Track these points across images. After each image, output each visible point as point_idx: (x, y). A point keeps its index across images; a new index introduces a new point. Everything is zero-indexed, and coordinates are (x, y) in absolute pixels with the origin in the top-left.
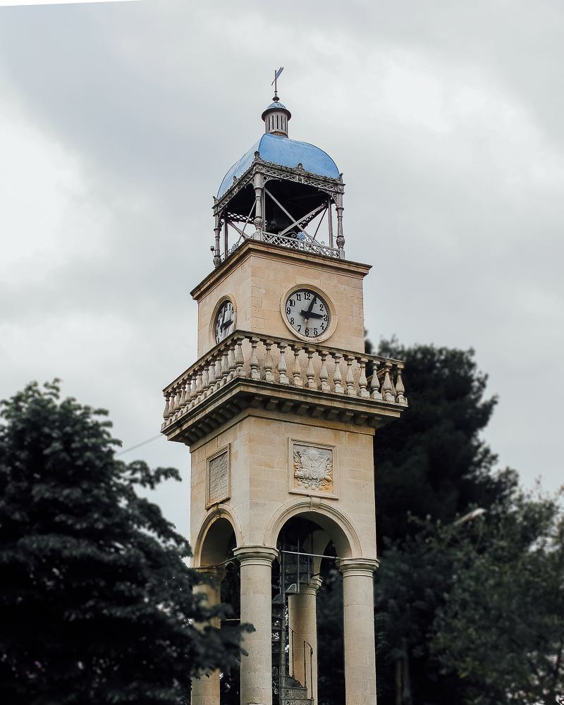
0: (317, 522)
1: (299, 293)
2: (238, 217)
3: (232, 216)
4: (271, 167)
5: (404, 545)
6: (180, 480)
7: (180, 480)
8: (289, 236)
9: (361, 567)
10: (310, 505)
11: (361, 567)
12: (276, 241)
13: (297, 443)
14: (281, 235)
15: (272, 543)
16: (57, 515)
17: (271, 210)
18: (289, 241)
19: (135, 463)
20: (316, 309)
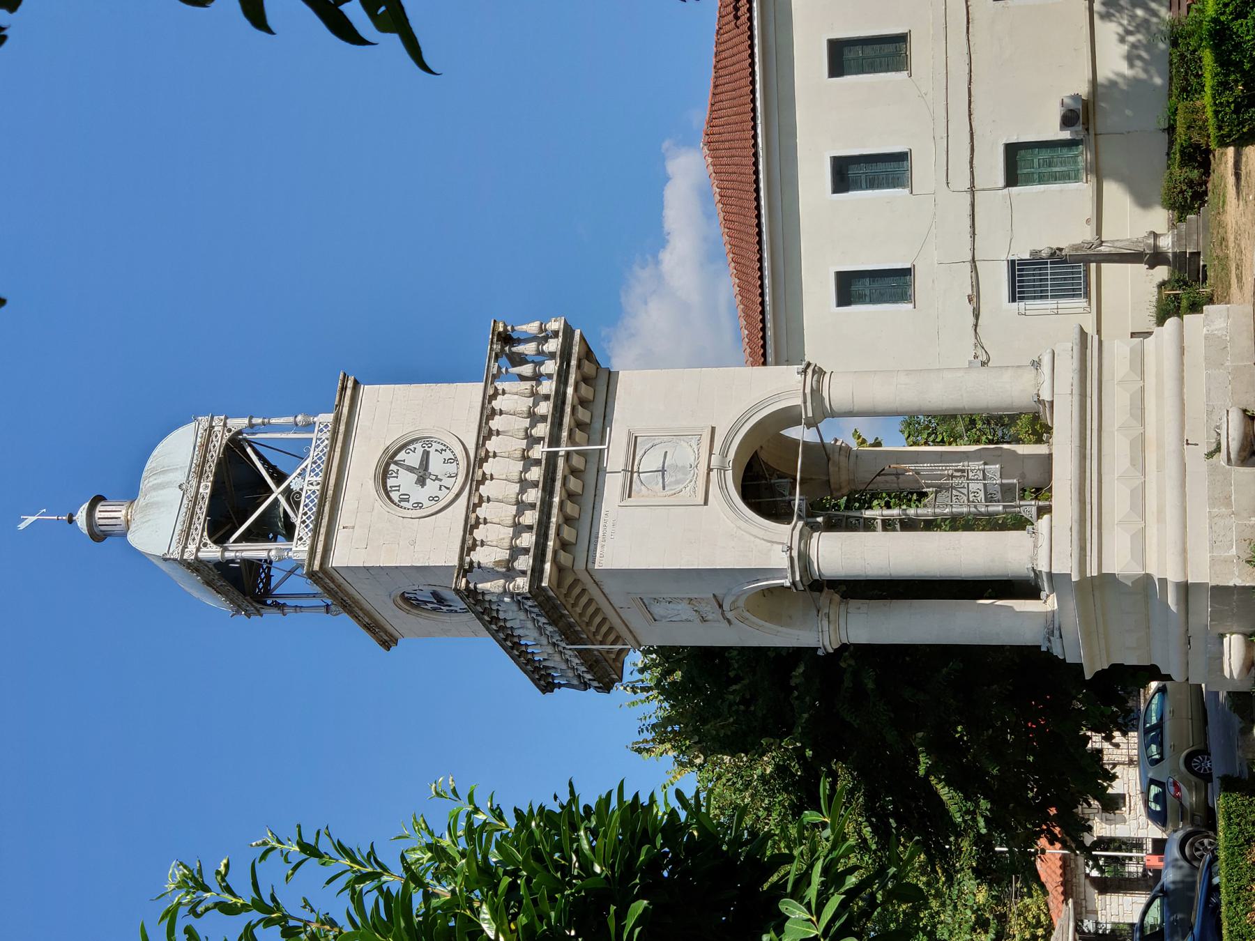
0: (746, 460)
1: (389, 489)
2: (263, 575)
3: (261, 585)
8: (298, 504)
12: (307, 526)
16: (1150, 876)
17: (259, 533)
18: (306, 506)
19: (520, 810)
20: (412, 458)
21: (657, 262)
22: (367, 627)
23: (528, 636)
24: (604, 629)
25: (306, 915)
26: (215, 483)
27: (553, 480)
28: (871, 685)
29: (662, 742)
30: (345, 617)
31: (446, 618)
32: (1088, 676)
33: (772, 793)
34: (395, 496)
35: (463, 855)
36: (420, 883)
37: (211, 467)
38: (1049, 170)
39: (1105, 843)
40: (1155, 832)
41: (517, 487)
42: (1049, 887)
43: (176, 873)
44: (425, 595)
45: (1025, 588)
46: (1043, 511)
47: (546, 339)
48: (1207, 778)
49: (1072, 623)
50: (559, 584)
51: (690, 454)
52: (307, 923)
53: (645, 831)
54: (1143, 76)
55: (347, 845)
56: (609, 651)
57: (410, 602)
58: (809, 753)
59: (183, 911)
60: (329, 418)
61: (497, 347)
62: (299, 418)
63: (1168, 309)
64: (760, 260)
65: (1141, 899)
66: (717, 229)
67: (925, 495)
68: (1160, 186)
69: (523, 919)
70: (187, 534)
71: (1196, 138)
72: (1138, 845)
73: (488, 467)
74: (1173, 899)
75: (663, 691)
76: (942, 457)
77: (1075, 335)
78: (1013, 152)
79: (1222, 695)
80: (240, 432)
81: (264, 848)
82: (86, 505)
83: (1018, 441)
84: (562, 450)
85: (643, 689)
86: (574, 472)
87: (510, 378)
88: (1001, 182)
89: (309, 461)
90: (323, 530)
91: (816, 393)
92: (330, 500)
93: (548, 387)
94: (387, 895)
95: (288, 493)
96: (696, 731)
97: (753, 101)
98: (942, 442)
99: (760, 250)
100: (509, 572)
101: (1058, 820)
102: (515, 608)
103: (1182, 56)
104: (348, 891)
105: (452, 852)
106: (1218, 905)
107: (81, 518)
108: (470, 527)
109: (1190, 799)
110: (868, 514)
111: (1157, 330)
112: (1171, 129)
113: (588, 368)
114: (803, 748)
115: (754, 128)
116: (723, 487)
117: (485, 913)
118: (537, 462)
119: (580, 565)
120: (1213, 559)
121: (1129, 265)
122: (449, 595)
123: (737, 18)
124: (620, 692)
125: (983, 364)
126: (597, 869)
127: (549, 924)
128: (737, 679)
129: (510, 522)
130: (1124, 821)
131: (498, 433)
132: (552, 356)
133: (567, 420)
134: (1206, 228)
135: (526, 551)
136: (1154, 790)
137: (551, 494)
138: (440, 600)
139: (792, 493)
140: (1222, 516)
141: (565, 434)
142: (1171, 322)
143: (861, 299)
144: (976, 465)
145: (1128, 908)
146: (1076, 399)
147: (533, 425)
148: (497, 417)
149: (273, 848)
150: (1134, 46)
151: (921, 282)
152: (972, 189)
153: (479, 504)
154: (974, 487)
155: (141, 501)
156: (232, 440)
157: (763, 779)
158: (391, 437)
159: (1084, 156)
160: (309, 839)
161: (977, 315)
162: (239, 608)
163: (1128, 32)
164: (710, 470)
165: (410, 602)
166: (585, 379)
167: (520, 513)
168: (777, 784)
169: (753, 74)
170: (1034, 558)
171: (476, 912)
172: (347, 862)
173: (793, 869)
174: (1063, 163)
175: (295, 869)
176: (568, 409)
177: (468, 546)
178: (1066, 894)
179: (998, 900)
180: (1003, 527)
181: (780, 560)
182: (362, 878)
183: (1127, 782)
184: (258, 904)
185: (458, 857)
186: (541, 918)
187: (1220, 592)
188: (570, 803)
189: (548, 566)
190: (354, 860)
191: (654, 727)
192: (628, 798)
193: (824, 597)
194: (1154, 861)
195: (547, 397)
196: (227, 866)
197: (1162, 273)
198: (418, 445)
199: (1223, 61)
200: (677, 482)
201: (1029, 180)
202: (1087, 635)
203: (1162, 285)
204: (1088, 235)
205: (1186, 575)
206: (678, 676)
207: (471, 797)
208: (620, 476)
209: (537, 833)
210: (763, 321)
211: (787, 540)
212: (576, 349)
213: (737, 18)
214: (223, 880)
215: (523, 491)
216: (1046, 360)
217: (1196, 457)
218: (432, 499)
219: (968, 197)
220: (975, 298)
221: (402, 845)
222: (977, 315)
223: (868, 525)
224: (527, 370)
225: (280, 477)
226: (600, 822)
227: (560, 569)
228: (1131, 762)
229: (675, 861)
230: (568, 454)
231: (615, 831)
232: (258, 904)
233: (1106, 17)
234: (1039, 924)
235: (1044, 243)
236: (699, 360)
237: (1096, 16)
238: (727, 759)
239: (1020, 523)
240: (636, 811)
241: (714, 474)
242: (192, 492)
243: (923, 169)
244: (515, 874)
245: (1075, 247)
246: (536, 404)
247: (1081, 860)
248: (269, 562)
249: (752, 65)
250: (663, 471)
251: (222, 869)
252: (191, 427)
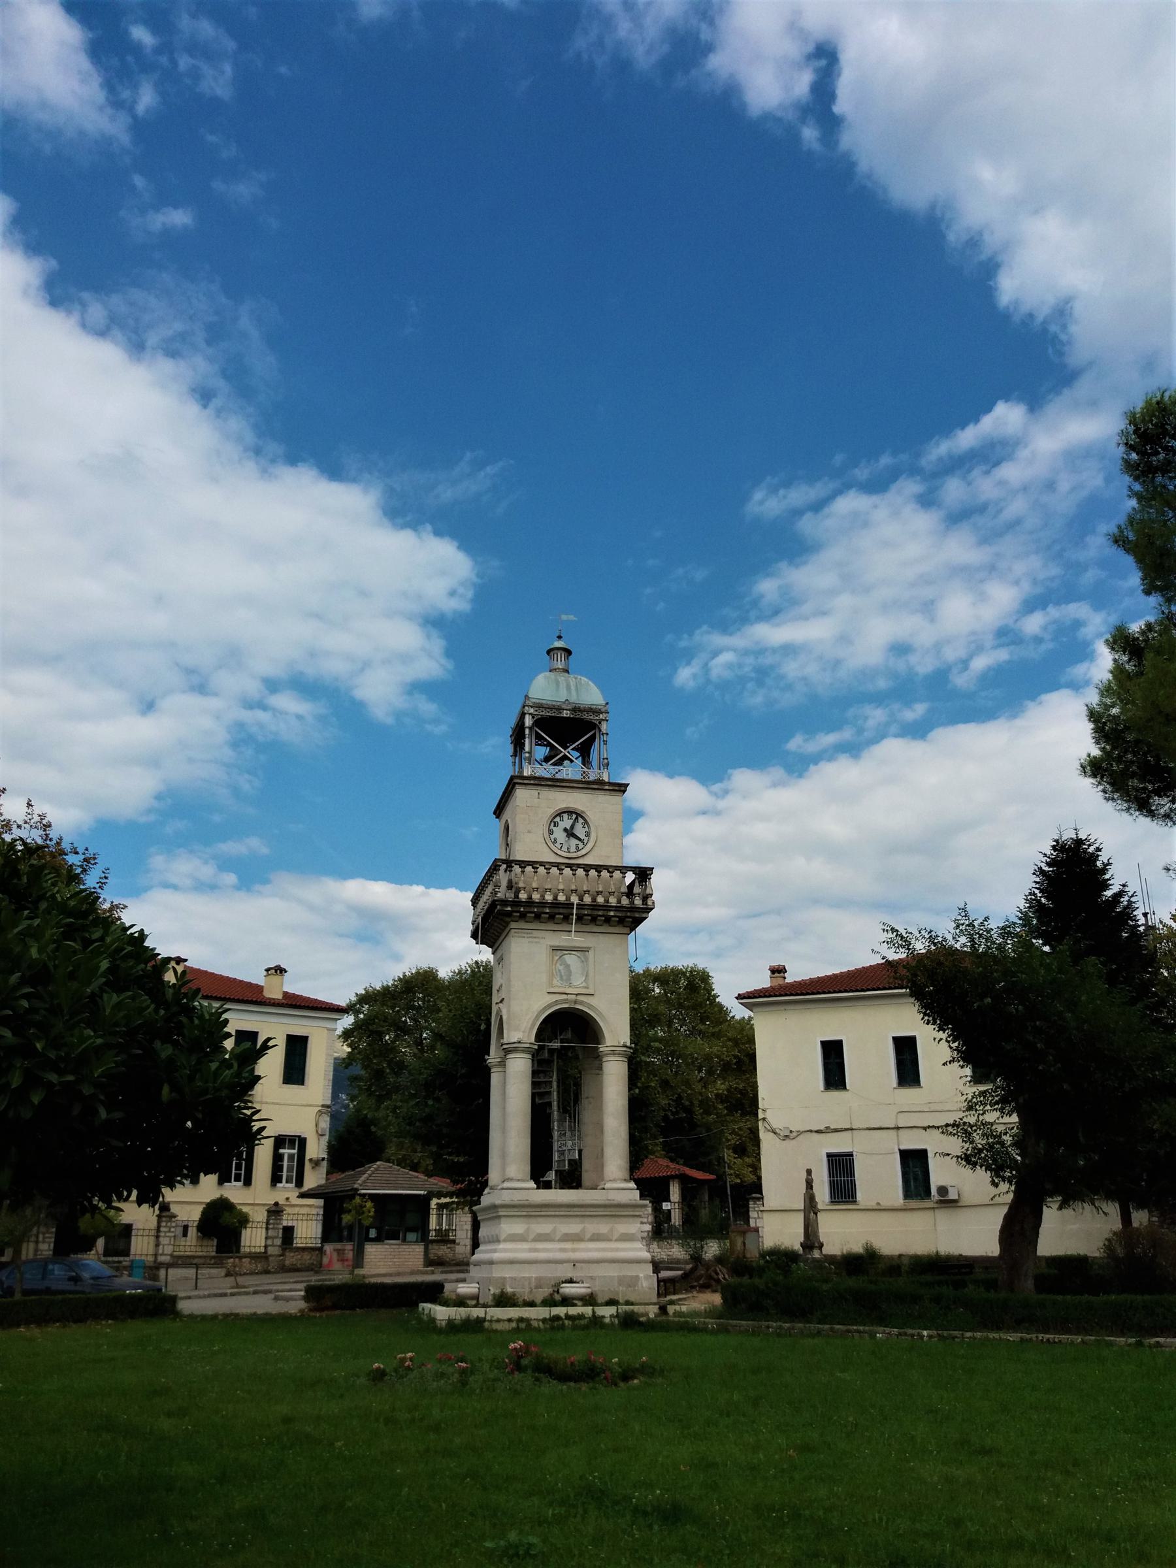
4: (539, 706)
5: (636, 890)
9: (613, 1053)
10: (566, 1001)
11: (613, 1053)
13: (555, 949)
34: (557, 819)
37: (578, 715)
38: (912, 1178)
88: (902, 1147)
116: (556, 1003)
120: (505, 1278)
121: (803, 1231)
132: (619, 901)
140: (530, 1283)
148: (584, 873)
151: (835, 1094)
152: (898, 1128)
156: (595, 724)
158: (590, 815)
161: (818, 1132)
174: (916, 1187)
220: (828, 1130)
222: (818, 1132)
242: (564, 706)
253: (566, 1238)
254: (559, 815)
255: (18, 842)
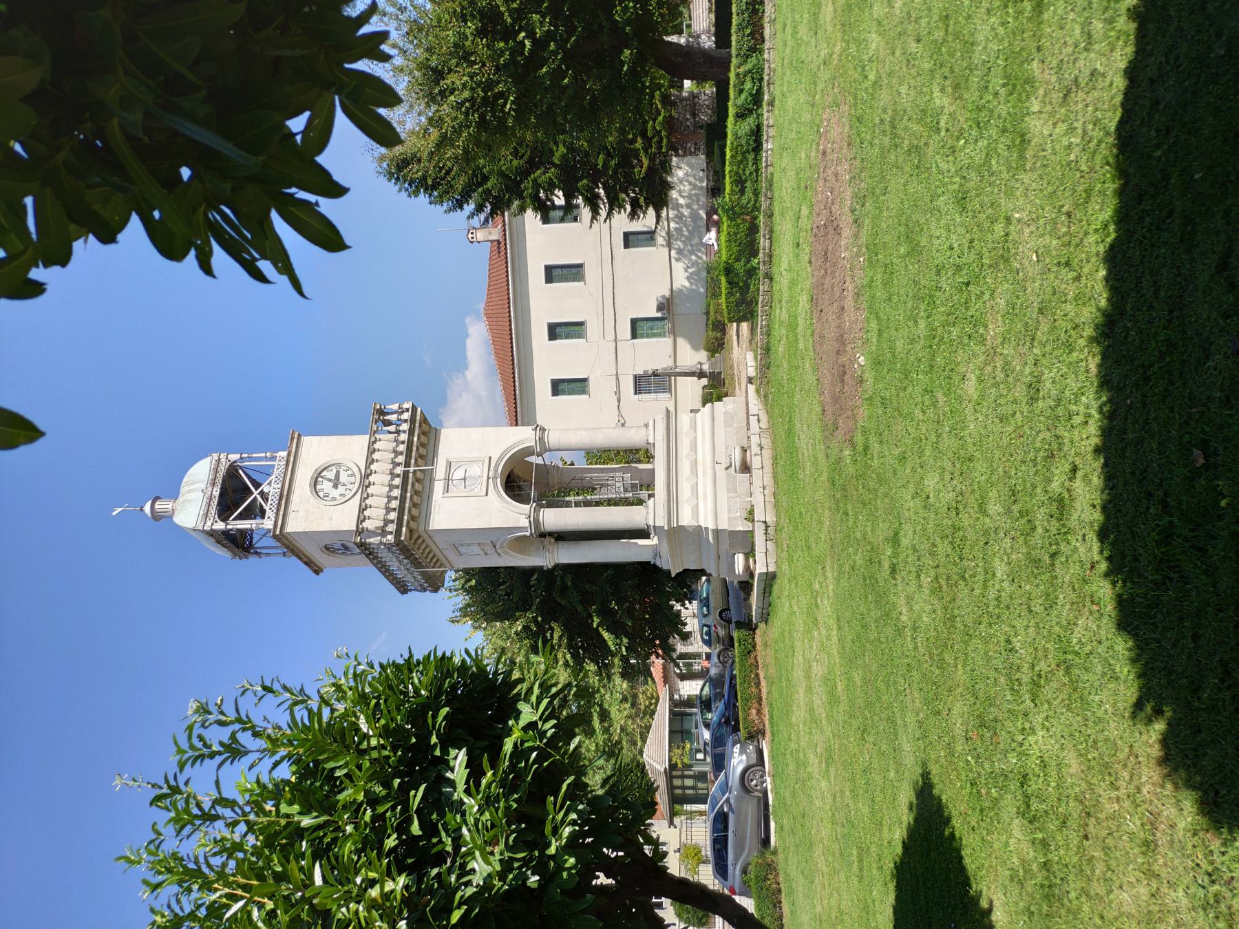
6: (214, 276)
7: (214, 276)
8: (267, 499)
14: (267, 508)
15: (525, 508)
17: (247, 515)
20: (330, 474)
21: (464, 376)
22: (306, 563)
23: (394, 565)
24: (434, 560)
25: (265, 724)
26: (221, 489)
27: (407, 485)
28: (570, 584)
29: (465, 617)
30: (294, 558)
31: (350, 557)
32: (673, 576)
33: (521, 640)
34: (321, 494)
35: (350, 689)
36: (327, 703)
37: (219, 481)
39: (683, 656)
40: (706, 649)
41: (387, 489)
42: (656, 680)
43: (193, 705)
44: (338, 546)
45: (643, 533)
46: (650, 496)
47: (402, 412)
48: (729, 622)
49: (665, 550)
50: (410, 539)
51: (477, 471)
52: (265, 729)
53: (448, 670)
54: (694, 287)
55: (288, 685)
56: (437, 572)
57: (329, 549)
58: (540, 619)
59: (197, 726)
60: (284, 454)
61: (376, 417)
62: (268, 454)
63: (707, 399)
64: (514, 373)
65: (700, 683)
66: (492, 360)
67: (596, 489)
68: (703, 340)
69: (383, 722)
70: (206, 516)
71: (719, 317)
72: (698, 656)
73: (372, 479)
74: (716, 683)
75: (465, 590)
76: (603, 471)
77: (665, 412)
78: (634, 322)
79: (735, 583)
80: (235, 462)
81: (242, 690)
82: (150, 502)
83: (640, 461)
84: (412, 469)
85: (455, 590)
86: (418, 480)
87: (383, 432)
88: (629, 337)
89: (273, 477)
90: (281, 513)
91: (542, 439)
92: (285, 497)
93: (404, 437)
94: (310, 711)
95: (262, 494)
96: (483, 610)
97: (508, 294)
98: (604, 463)
99: (513, 368)
100: (383, 532)
101: (660, 646)
102: (386, 551)
103: (712, 278)
104: (288, 711)
105: (345, 688)
106: (735, 685)
107: (147, 509)
108: (362, 510)
109: (722, 632)
110: (568, 499)
111: (702, 409)
112: (708, 313)
113: (424, 426)
114: (537, 616)
115: (509, 307)
116: (495, 487)
117: (362, 719)
118: (398, 476)
119: (421, 528)
120: (729, 518)
122: (351, 545)
123: (499, 252)
124: (443, 592)
125: (623, 425)
126: (423, 692)
127: (396, 723)
128: (503, 584)
129: (384, 506)
130: (692, 644)
131: (377, 461)
132: (406, 421)
133: (414, 454)
134: (724, 361)
135: (392, 521)
136: (705, 629)
137: (406, 492)
138: (346, 548)
139: (530, 489)
141: (413, 461)
142: (708, 405)
143: (564, 393)
144: (619, 474)
145: (694, 686)
146: (665, 442)
147: (396, 457)
149: (248, 689)
150: (691, 274)
151: (592, 385)
152: (616, 340)
153: (367, 498)
154: (618, 485)
155: (181, 499)
157: (517, 633)
159: (668, 326)
160: (268, 683)
161: (619, 401)
162: (235, 555)
163: (688, 267)
164: (488, 478)
165: (329, 549)
166: (424, 433)
167: (389, 502)
168: (523, 635)
169: (508, 281)
170: (647, 519)
171: (358, 718)
172: (288, 695)
173: (525, 686)
175: (260, 700)
176: (414, 449)
177: (361, 519)
178: (666, 681)
179: (632, 687)
180: (632, 504)
181: (524, 523)
182: (296, 703)
183: (692, 625)
184: (239, 720)
185: (347, 690)
186: (392, 720)
187: (733, 533)
188: (409, 658)
189: (404, 529)
190: (292, 694)
191: (461, 609)
192: (439, 654)
193: (548, 540)
194: (706, 664)
195: (403, 442)
196: (222, 700)
197: (704, 381)
198: (334, 468)
199: (730, 283)
200: (472, 485)
201: (642, 336)
202: (672, 556)
203: (704, 387)
204: (670, 363)
205: (717, 525)
206: (473, 582)
207: (356, 658)
208: (442, 482)
209: (390, 675)
210: (515, 403)
211: (528, 513)
212: (418, 418)
213: (499, 252)
214: (219, 708)
215: (390, 490)
216: (651, 423)
217: (720, 469)
218: (341, 495)
219: (614, 344)
220: (618, 393)
221: (319, 685)
222: (619, 401)
223: (568, 505)
224: (392, 428)
225: (257, 485)
226: (425, 668)
227: (411, 531)
228: (694, 615)
229: (465, 685)
230: (415, 471)
231: (432, 672)
232: (239, 720)
233: (678, 260)
234: (653, 697)
235: (650, 368)
236: (486, 424)
237: (673, 260)
238: (498, 624)
239: (640, 502)
240: (444, 660)
241: (491, 480)
243: (592, 329)
244: (378, 698)
245: (665, 369)
246: (397, 446)
247: (672, 665)
248: (252, 530)
249: (507, 276)
250: (464, 479)
251: (219, 702)
252: (209, 459)
253: (695, 472)
254: (317, 493)
255: (231, 872)
